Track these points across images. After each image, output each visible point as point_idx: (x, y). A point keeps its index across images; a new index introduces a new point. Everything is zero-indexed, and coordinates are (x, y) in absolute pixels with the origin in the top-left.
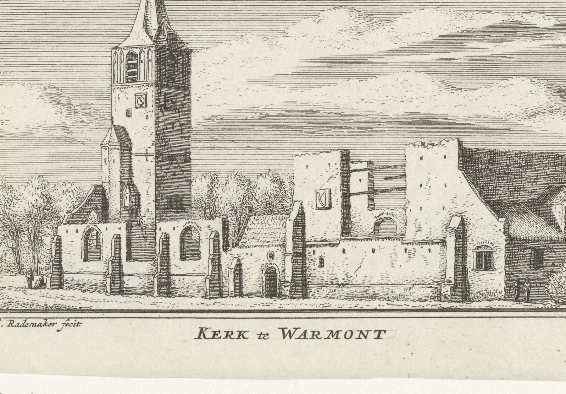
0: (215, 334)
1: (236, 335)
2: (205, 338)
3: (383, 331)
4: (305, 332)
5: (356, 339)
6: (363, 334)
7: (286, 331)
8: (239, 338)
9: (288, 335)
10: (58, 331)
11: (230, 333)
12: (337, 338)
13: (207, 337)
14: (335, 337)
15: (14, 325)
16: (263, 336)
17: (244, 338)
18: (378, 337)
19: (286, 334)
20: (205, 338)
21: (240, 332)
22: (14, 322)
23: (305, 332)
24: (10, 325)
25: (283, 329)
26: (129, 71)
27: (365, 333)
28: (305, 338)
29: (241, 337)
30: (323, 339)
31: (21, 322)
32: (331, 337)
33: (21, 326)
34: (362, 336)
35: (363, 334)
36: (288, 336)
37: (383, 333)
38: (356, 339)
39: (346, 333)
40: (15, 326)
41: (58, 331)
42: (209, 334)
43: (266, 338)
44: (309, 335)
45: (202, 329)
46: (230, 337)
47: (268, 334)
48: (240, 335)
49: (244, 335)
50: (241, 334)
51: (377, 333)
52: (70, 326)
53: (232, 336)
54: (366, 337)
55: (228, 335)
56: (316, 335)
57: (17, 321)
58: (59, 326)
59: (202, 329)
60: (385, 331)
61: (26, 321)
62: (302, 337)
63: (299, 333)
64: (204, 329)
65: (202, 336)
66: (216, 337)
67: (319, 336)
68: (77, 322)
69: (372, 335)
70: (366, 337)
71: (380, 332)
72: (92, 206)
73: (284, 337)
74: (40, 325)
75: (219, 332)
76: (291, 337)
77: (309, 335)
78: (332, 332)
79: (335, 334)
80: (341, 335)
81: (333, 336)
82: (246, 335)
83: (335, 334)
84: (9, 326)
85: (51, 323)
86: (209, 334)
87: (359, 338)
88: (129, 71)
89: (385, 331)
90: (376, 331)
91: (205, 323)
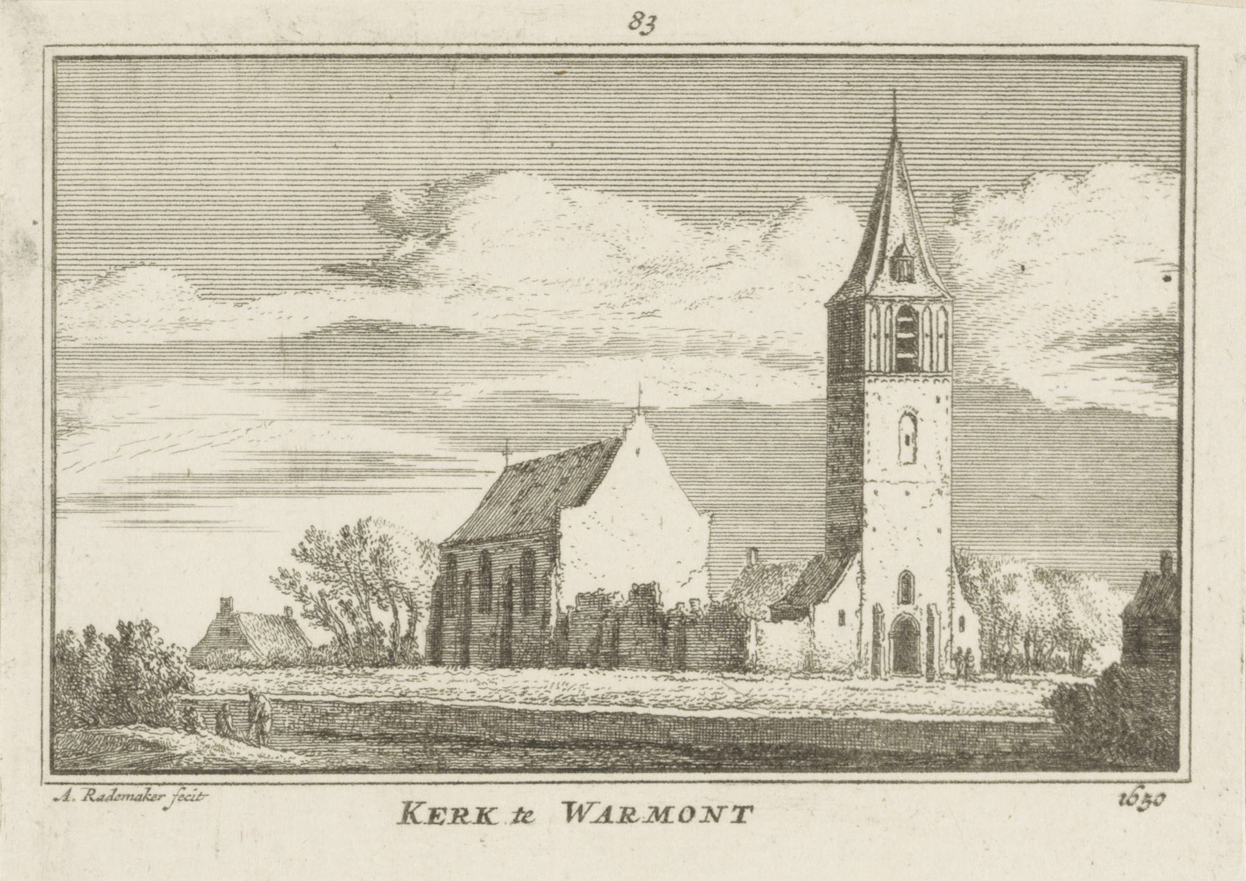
0: (434, 814)
1: (473, 815)
2: (415, 822)
3: (748, 807)
4: (609, 809)
5: (701, 822)
6: (713, 814)
7: (575, 808)
8: (479, 821)
9: (577, 815)
10: (165, 809)
11: (462, 812)
12: (666, 821)
13: (418, 819)
14: (662, 819)
15: (94, 797)
16: (522, 816)
17: (488, 822)
18: (740, 820)
19: (573, 811)
20: (415, 822)
21: (481, 810)
22: (94, 790)
23: (609, 809)
24: (88, 798)
25: (570, 804)
26: (911, 335)
27: (716, 812)
28: (607, 820)
29: (409, 820)
30: (422, 825)
31: (107, 791)
32: (653, 819)
33: (106, 800)
34: (710, 818)
35: (713, 814)
36: (576, 818)
37: (747, 812)
38: (701, 822)
39: (682, 812)
40: (98, 800)
41: (165, 809)
42: (423, 814)
43: (528, 819)
44: (616, 815)
45: (409, 804)
46: (462, 820)
47: (531, 812)
48: (480, 816)
49: (490, 815)
50: (484, 816)
51: (738, 810)
52: (186, 800)
53: (466, 819)
54: (716, 819)
55: (460, 815)
56: (627, 816)
57: (100, 790)
58: (165, 802)
59: (409, 804)
60: (752, 808)
61: (116, 790)
62: (603, 819)
63: (597, 812)
64: (413, 806)
65: (483, 820)
66: (436, 820)
67: (633, 818)
68: (197, 793)
69: (729, 815)
70: (716, 819)
71: (742, 809)
72: (753, 562)
73: (569, 818)
74: (140, 798)
75: (445, 810)
76: (580, 820)
77: (616, 815)
78: (656, 810)
79: (660, 815)
80: (674, 815)
81: (657, 818)
82: (492, 816)
83: (660, 815)
84: (85, 800)
85: (156, 795)
86: (423, 814)
87: (706, 821)
88: (911, 335)
89: (752, 808)
90: (735, 807)
91: (415, 794)
